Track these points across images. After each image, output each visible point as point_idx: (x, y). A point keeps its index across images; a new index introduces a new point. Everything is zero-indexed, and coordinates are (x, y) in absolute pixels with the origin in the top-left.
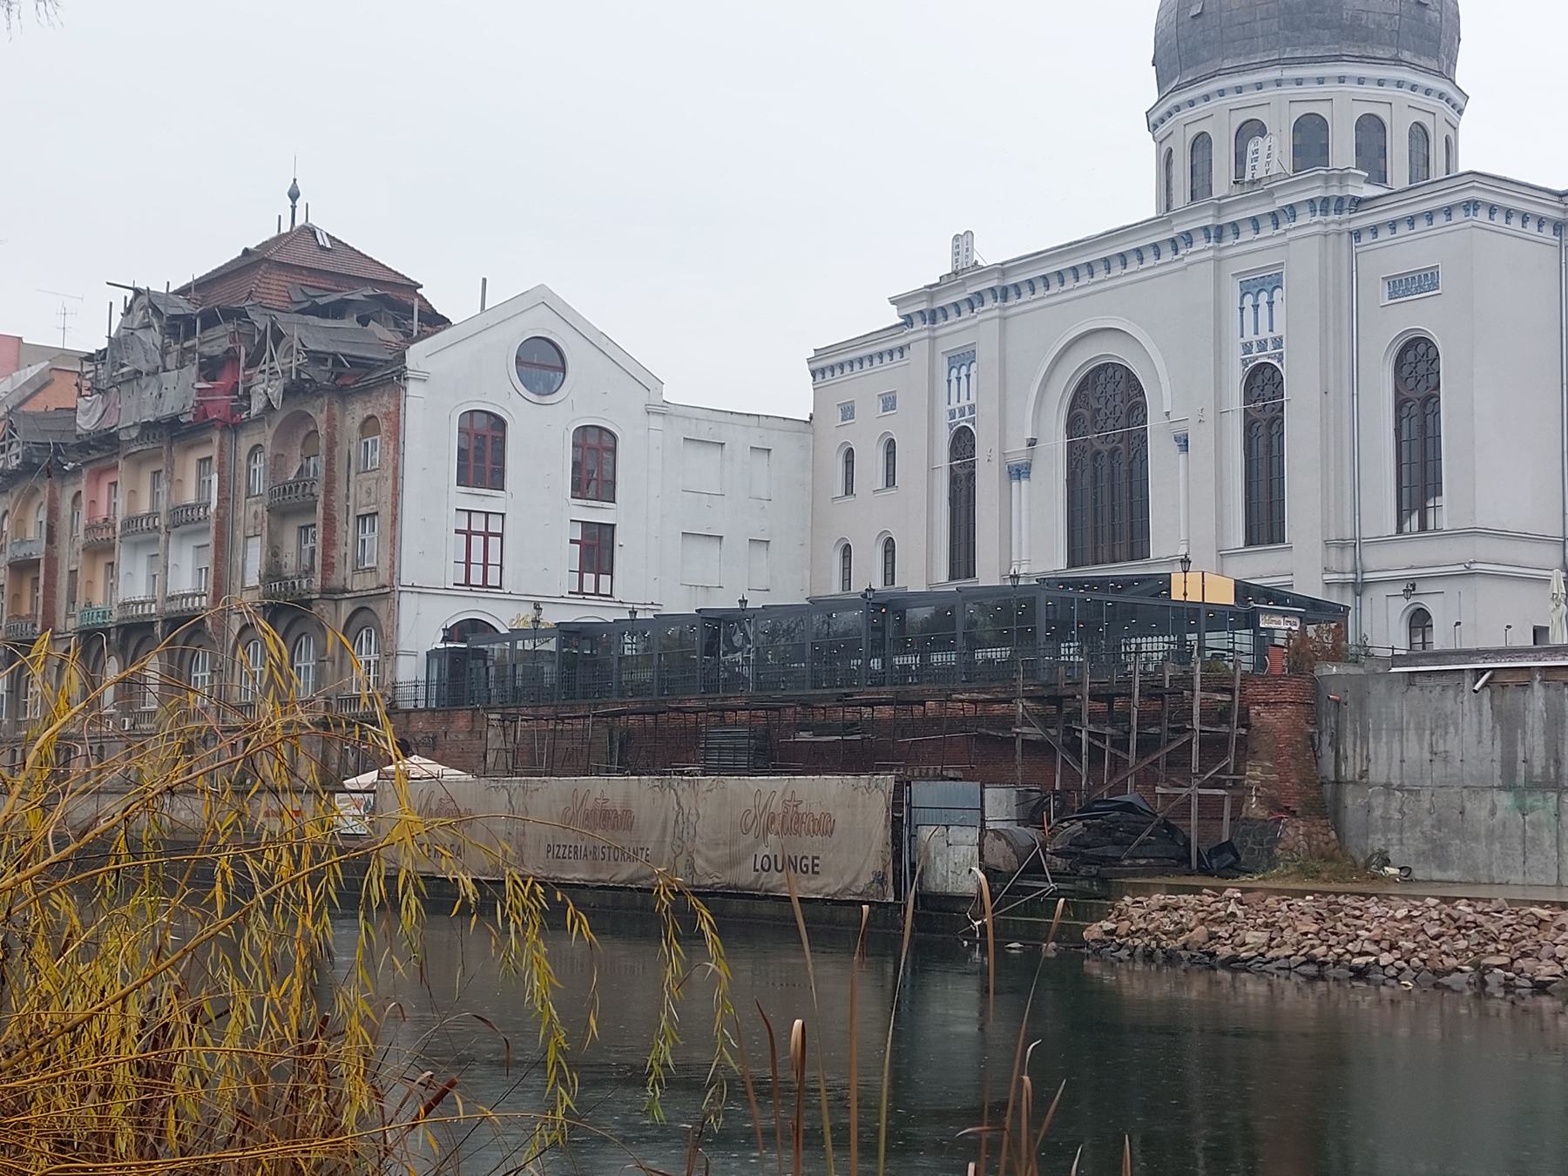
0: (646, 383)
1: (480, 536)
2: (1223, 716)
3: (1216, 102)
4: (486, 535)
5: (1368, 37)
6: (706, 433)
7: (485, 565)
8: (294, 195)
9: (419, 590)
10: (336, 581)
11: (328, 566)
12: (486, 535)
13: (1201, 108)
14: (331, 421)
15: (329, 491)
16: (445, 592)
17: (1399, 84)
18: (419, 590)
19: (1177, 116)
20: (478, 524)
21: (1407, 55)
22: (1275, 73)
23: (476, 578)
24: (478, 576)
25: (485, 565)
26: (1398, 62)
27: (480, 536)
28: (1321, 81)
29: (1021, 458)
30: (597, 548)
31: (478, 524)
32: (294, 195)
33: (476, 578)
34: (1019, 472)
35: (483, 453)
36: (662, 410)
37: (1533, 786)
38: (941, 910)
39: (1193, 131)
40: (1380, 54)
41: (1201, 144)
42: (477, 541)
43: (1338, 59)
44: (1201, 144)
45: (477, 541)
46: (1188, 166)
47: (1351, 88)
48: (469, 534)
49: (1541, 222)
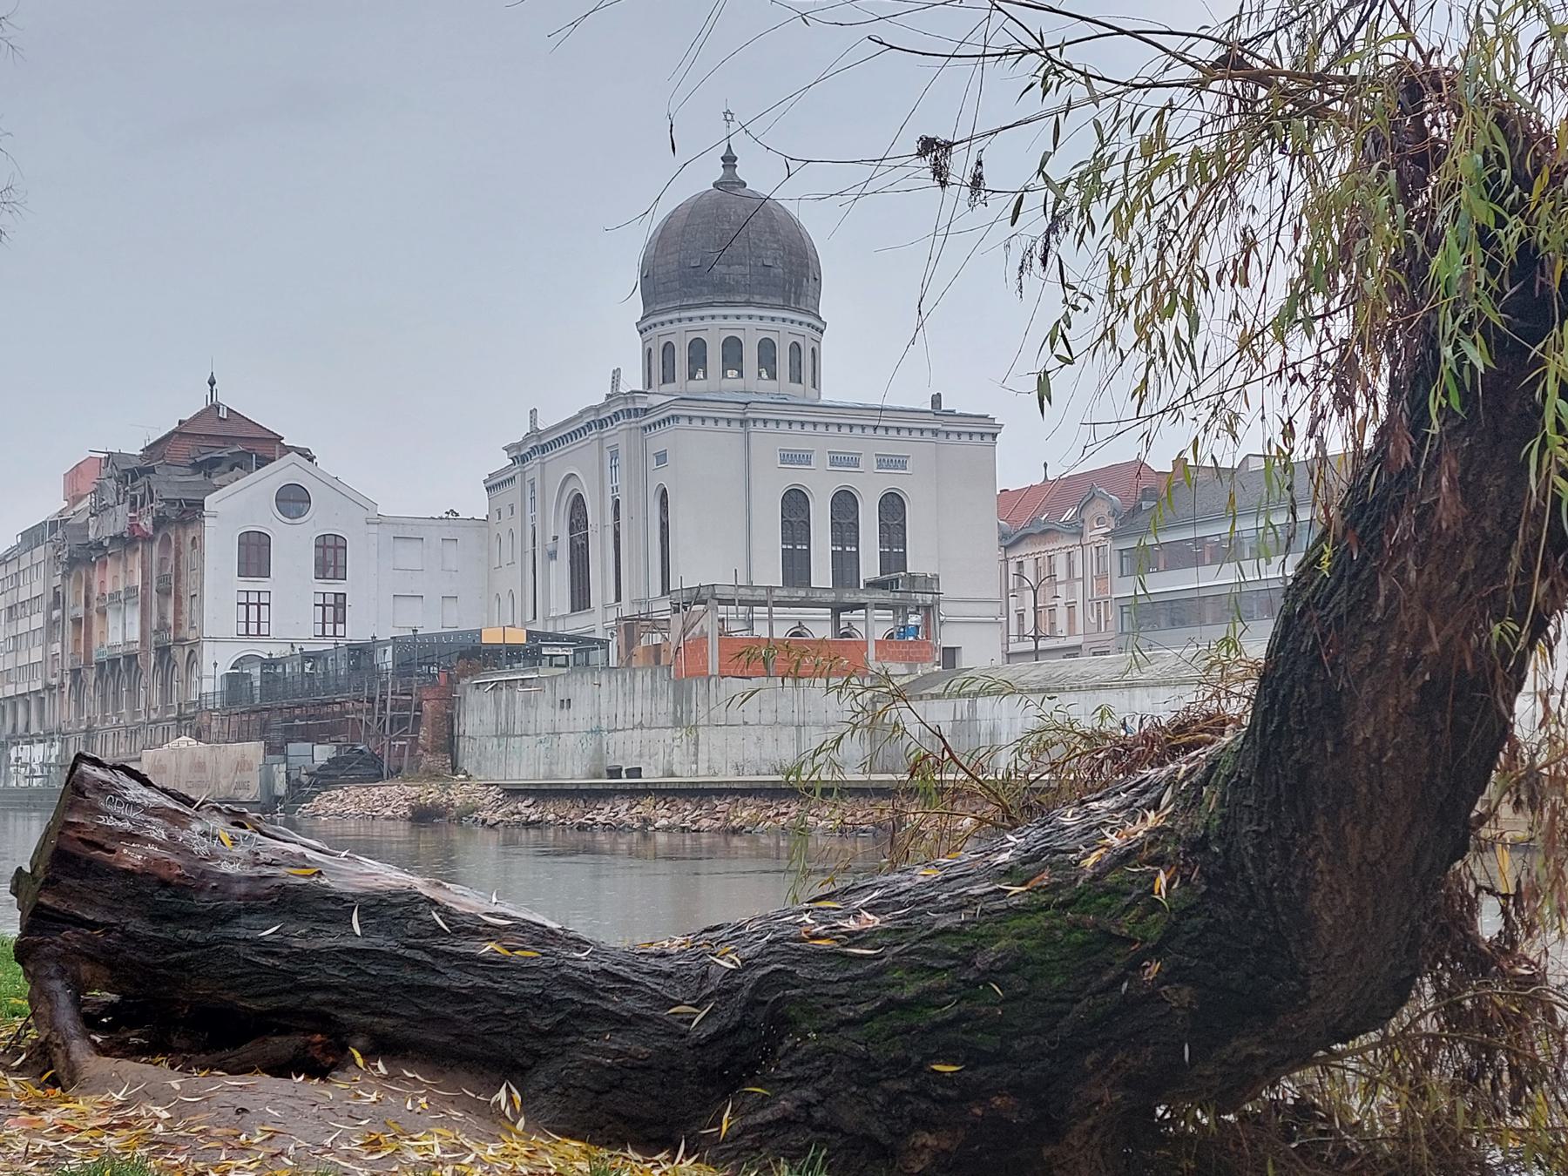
0: (364, 504)
1: (253, 606)
2: (406, 706)
3: (676, 325)
4: (259, 605)
5: (731, 290)
6: (405, 532)
7: (259, 623)
8: (212, 383)
9: (215, 640)
10: (182, 635)
11: (178, 625)
12: (259, 605)
13: (668, 327)
14: (177, 538)
15: (177, 581)
16: (231, 640)
17: (750, 317)
18: (215, 640)
19: (654, 330)
20: (253, 598)
21: (757, 298)
22: (676, 315)
23: (253, 629)
24: (253, 629)
25: (259, 623)
26: (748, 304)
27: (253, 606)
28: (702, 318)
29: (550, 548)
30: (337, 608)
31: (253, 598)
32: (212, 383)
33: (253, 629)
34: (553, 555)
35: (255, 554)
36: (380, 521)
37: (502, 735)
38: (278, 799)
39: (663, 341)
40: (738, 299)
41: (668, 349)
42: (253, 609)
43: (710, 305)
44: (668, 349)
45: (253, 609)
46: (661, 363)
47: (719, 322)
48: (247, 605)
49: (729, 421)
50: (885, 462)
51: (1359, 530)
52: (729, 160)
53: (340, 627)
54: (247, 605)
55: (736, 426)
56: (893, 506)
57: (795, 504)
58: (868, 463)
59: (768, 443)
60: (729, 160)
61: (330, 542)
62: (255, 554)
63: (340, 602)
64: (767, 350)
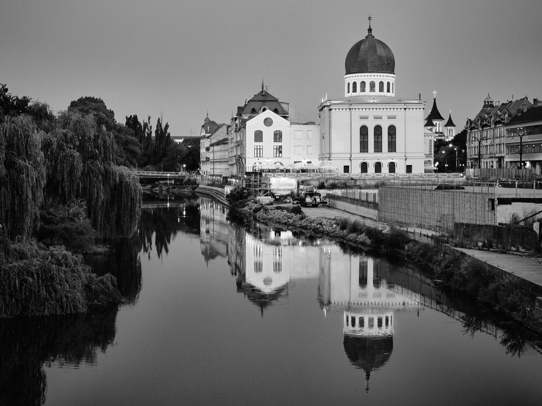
4: (260, 149)
12: (260, 149)
23: (258, 155)
33: (258, 155)
35: (259, 136)
42: (258, 150)
45: (258, 150)
50: (389, 118)
51: (35, 179)
52: (370, 30)
53: (280, 154)
54: (257, 149)
55: (348, 110)
56: (392, 130)
57: (364, 130)
58: (385, 118)
59: (357, 113)
60: (370, 30)
61: (278, 132)
62: (259, 136)
63: (280, 147)
64: (372, 85)
